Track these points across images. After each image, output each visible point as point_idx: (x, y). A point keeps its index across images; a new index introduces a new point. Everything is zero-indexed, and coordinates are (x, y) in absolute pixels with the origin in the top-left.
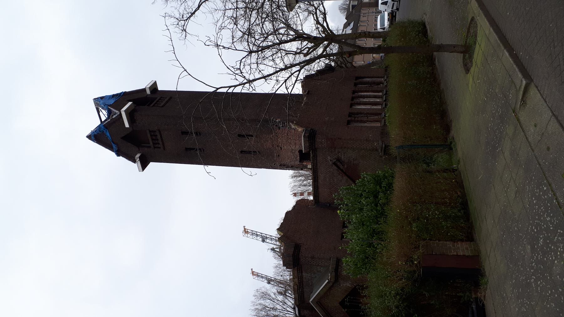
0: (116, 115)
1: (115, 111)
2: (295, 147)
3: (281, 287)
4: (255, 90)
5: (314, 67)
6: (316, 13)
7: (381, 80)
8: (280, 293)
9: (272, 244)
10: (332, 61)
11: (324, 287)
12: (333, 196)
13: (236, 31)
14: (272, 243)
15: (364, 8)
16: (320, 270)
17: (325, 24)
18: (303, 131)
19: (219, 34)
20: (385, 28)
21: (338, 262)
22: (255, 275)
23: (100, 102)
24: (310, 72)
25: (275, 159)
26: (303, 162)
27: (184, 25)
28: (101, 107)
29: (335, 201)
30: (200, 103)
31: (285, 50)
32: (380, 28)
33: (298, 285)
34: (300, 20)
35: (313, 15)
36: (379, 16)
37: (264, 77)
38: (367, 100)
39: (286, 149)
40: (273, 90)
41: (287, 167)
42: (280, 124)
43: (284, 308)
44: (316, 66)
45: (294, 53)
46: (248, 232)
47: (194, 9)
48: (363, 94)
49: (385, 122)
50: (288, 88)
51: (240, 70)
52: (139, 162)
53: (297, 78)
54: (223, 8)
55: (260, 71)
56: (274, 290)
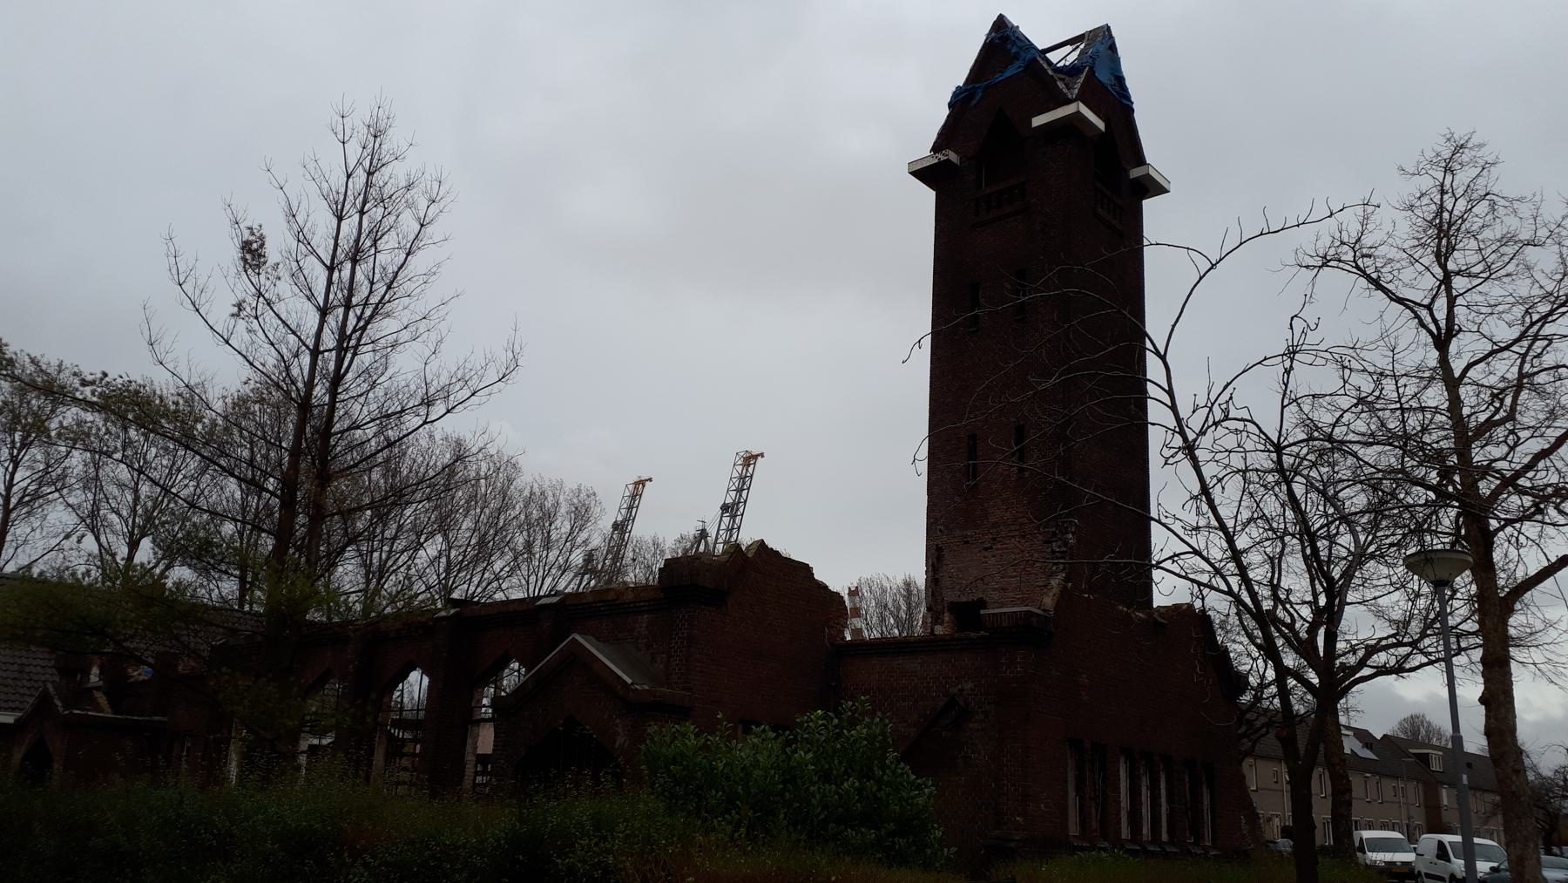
0: (1065, 90)
1: (1078, 86)
2: (994, 590)
3: (605, 559)
4: (1166, 464)
5: (1234, 641)
6: (1400, 644)
7: (1207, 839)
8: (589, 557)
9: (718, 533)
10: (1256, 694)
11: (613, 671)
12: (862, 697)
13: (1333, 408)
14: (721, 532)
15: (1421, 792)
16: (656, 662)
17: (1366, 672)
18: (1044, 610)
19: (1327, 355)
20: (1365, 853)
21: (679, 712)
22: (636, 488)
23: (1100, 44)
24: (1219, 630)
25: (958, 533)
26: (951, 614)
27: (1340, 261)
28: (1087, 47)
29: (850, 703)
30: (1119, 311)
31: (1282, 553)
32: (1361, 839)
33: (617, 602)
34: (1375, 598)
35: (1393, 636)
36: (1399, 835)
37: (1205, 490)
38: (1144, 799)
39: (986, 563)
40: (1166, 517)
41: (933, 565)
42: (1059, 543)
43: (550, 568)
44: (1240, 648)
45: (1275, 582)
46: (749, 465)
47: (1390, 287)
48: (1163, 784)
49: (1082, 849)
50: (1174, 562)
51: (1223, 421)
52: (936, 161)
53: (1206, 586)
54: (1400, 370)
55: (1220, 480)
56: (596, 541)
